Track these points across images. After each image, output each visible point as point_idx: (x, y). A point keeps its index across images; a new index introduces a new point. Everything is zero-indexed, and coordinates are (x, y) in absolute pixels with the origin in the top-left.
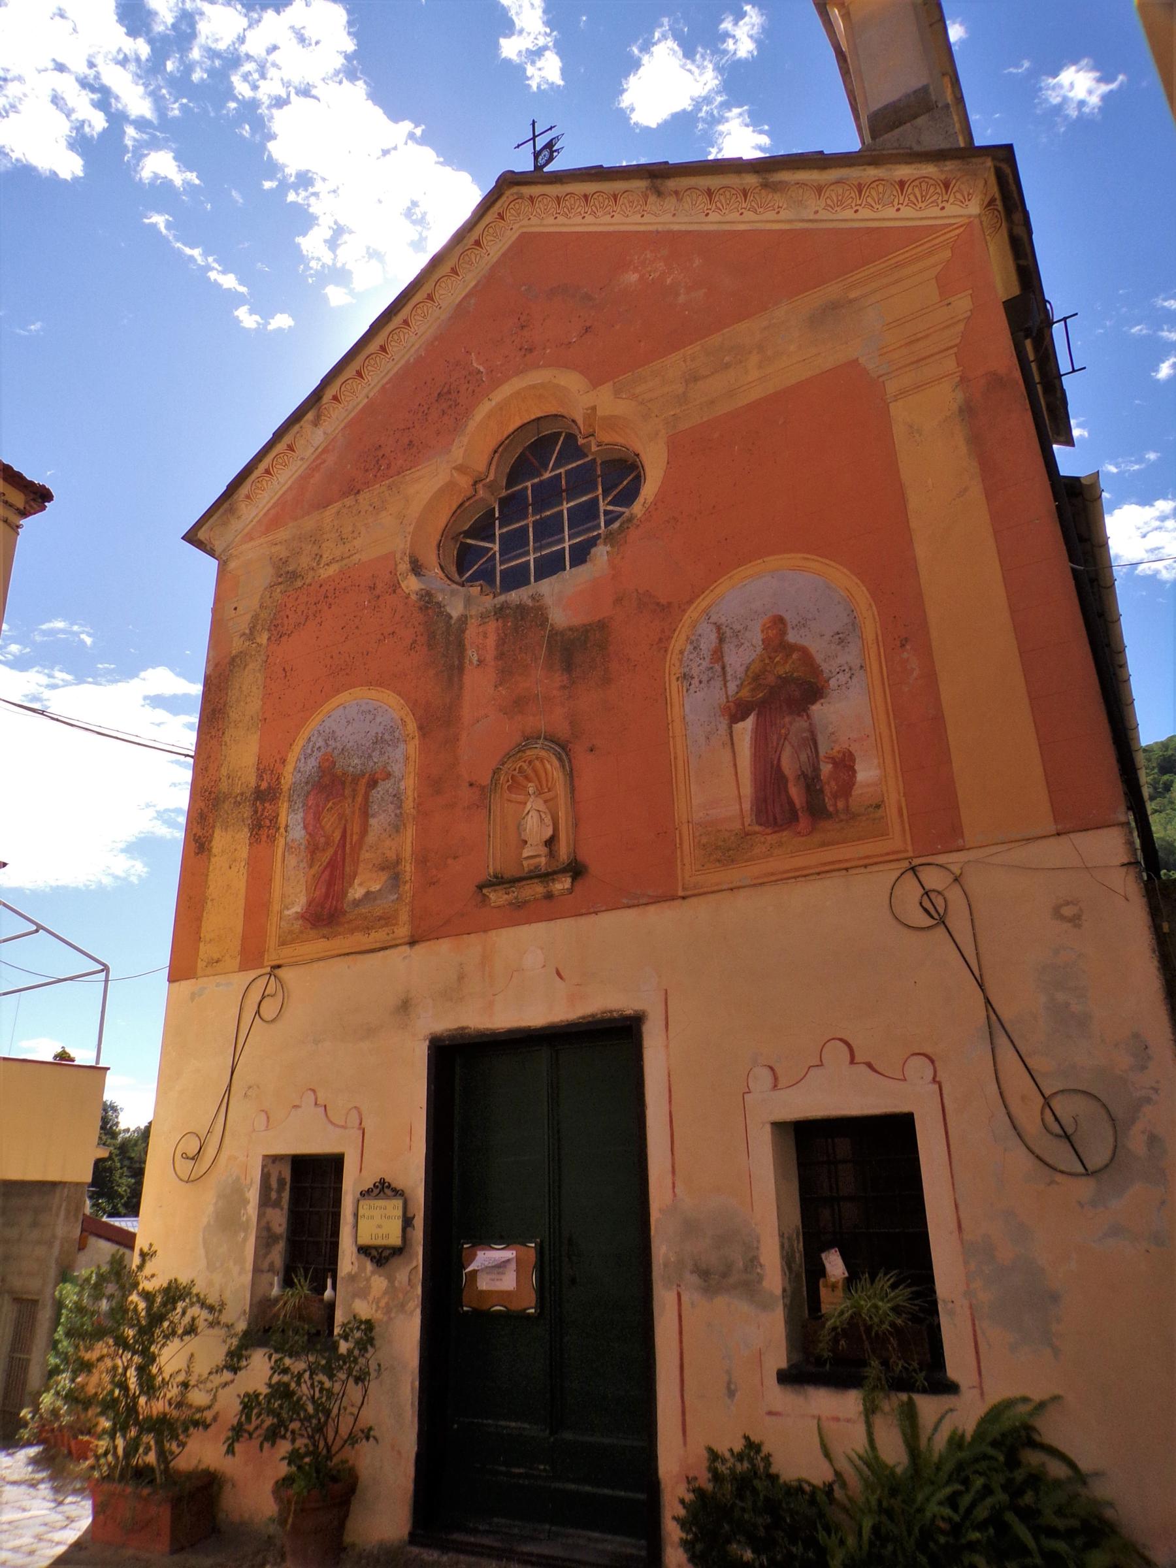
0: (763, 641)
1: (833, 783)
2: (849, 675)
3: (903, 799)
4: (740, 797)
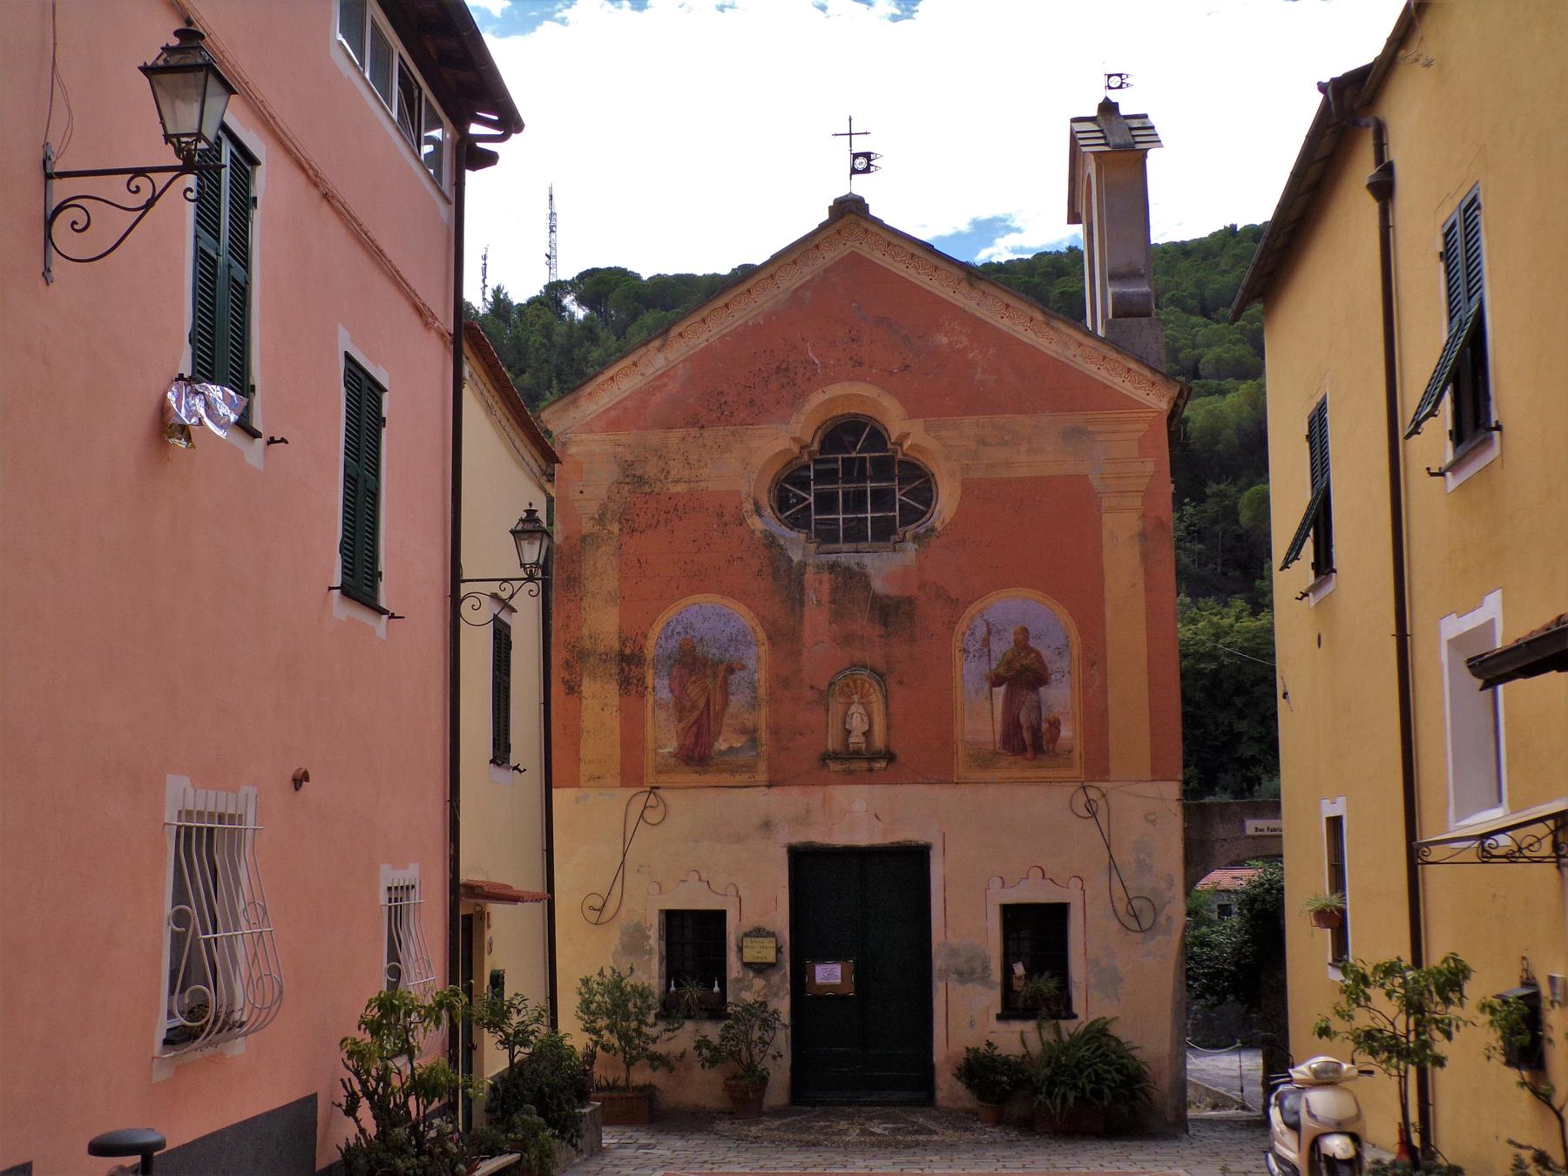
0: (1015, 641)
1: (1048, 734)
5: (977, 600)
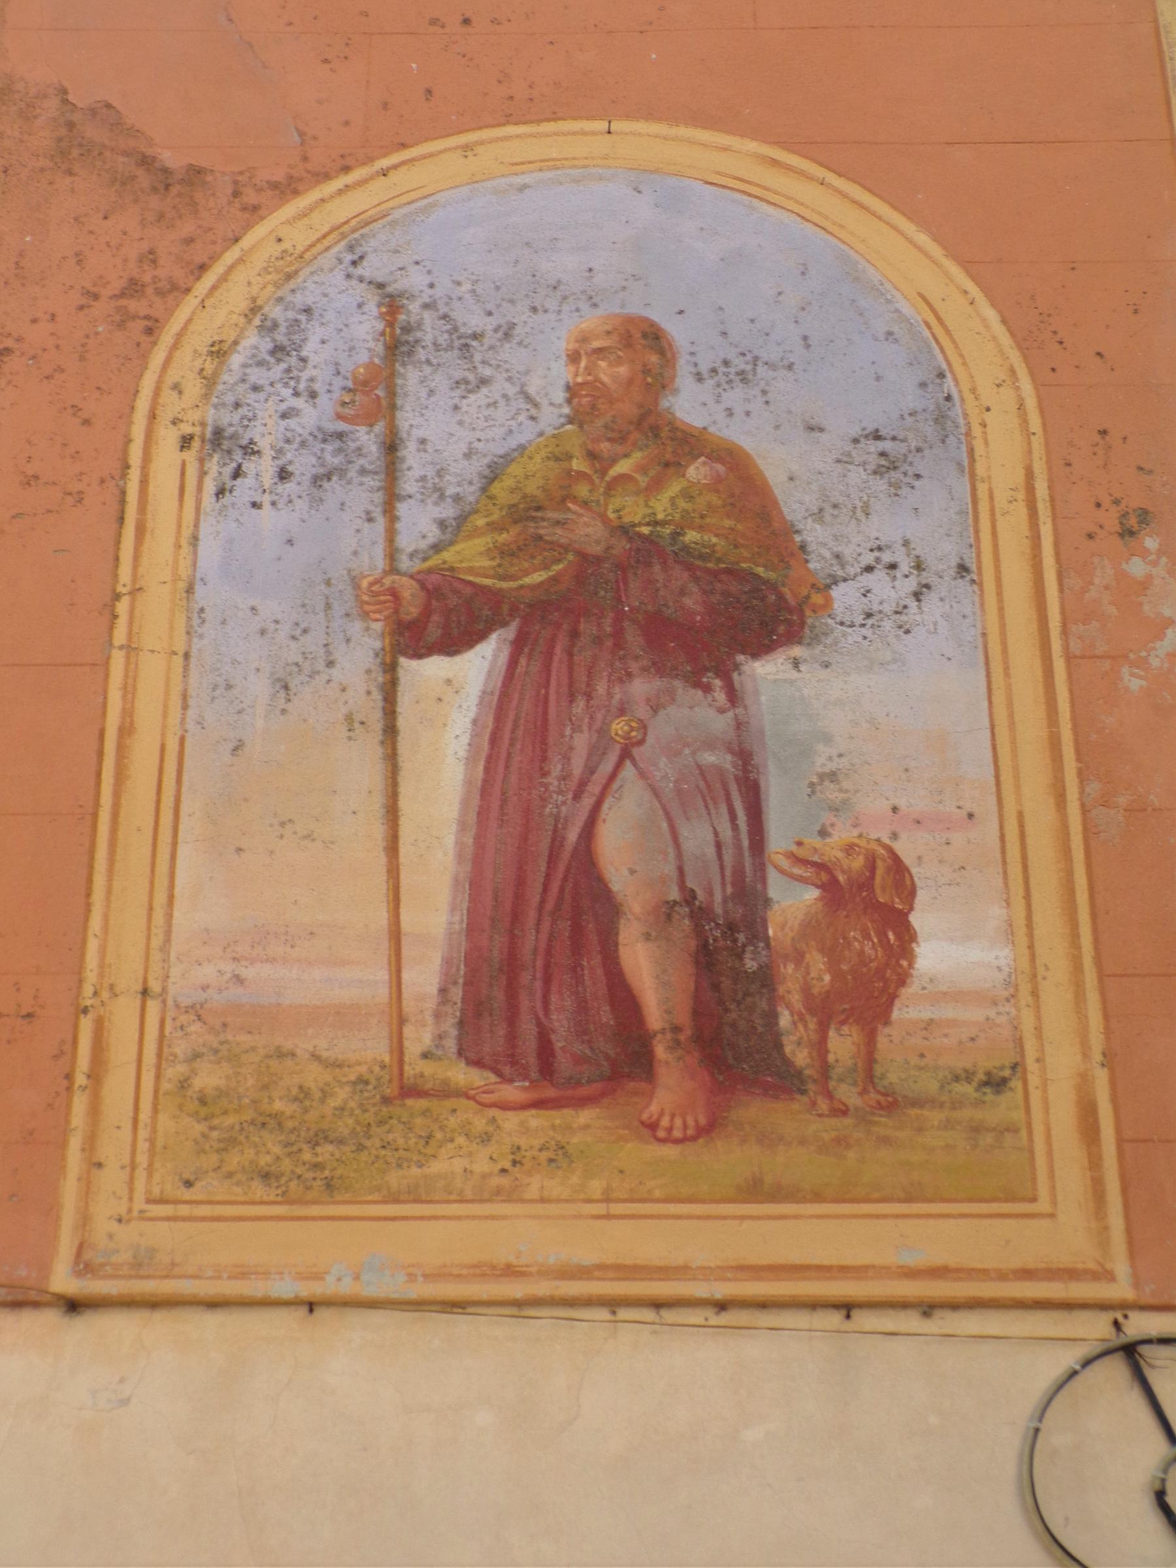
0: (572, 391)
1: (817, 962)
2: (911, 584)
3: (1101, 1078)
4: (396, 934)
5: (325, 176)
